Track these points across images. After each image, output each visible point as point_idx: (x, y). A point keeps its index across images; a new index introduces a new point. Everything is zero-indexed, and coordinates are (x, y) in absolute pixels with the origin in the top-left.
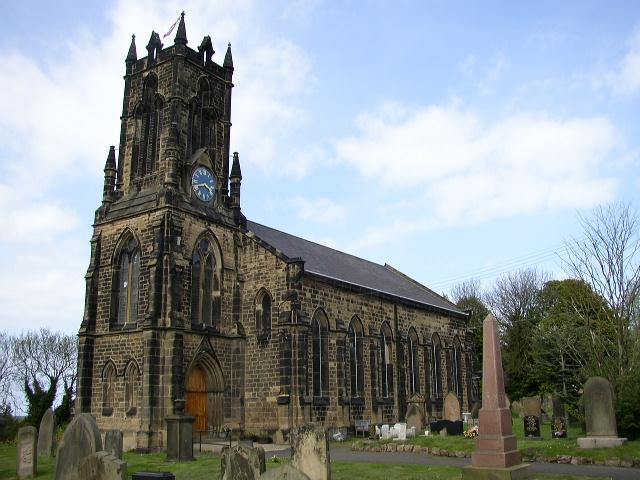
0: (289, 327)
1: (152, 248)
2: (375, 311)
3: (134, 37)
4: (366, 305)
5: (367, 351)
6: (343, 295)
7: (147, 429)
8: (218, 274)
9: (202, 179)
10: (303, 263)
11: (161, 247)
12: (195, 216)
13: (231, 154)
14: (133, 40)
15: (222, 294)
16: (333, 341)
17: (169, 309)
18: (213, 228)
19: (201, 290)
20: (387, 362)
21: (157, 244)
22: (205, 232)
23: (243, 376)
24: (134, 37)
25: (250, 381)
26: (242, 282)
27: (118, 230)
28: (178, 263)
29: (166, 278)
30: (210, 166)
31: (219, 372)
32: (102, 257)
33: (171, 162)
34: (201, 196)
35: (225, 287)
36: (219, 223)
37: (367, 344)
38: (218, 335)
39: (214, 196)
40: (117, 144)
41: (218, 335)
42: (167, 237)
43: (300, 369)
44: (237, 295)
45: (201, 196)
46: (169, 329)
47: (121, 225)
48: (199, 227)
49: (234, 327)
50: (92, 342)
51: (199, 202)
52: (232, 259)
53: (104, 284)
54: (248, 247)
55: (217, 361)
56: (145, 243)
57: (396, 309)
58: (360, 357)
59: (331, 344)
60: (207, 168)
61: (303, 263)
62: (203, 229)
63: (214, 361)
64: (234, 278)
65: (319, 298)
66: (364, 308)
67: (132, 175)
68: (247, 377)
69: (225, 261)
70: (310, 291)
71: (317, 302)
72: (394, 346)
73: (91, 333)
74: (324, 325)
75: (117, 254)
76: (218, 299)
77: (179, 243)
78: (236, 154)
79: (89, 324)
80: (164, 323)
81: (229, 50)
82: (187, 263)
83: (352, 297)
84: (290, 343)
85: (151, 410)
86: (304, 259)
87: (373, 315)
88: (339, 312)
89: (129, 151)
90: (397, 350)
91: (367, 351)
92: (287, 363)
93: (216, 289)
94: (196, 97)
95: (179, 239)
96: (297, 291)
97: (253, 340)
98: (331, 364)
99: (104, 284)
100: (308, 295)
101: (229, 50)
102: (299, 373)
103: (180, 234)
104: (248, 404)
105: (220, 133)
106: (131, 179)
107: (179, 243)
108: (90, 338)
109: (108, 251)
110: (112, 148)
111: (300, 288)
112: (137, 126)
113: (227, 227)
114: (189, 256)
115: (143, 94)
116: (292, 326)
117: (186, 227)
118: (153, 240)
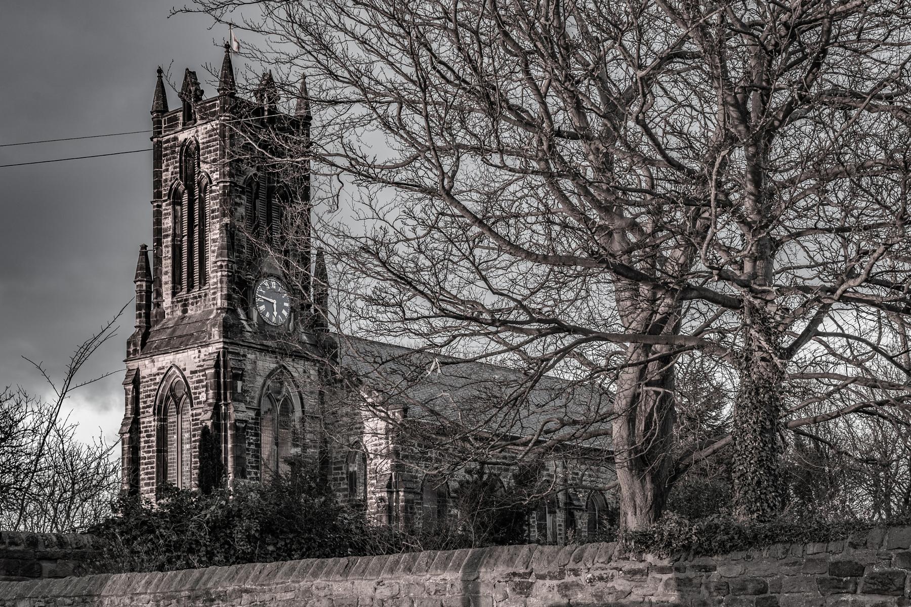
1: (204, 394)
3: (160, 71)
9: (271, 293)
11: (218, 396)
14: (160, 77)
17: (231, 477)
18: (288, 363)
19: (312, 290)
21: (211, 392)
22: (277, 369)
24: (160, 71)
27: (160, 369)
29: (226, 436)
32: (141, 405)
33: (225, 279)
39: (290, 315)
47: (164, 360)
48: (267, 364)
53: (146, 442)
56: (196, 388)
62: (273, 366)
67: (174, 288)
77: (239, 390)
82: (252, 414)
95: (239, 383)
99: (146, 442)
106: (174, 294)
107: (239, 390)
109: (149, 396)
115: (181, 167)
117: (249, 367)
118: (206, 386)
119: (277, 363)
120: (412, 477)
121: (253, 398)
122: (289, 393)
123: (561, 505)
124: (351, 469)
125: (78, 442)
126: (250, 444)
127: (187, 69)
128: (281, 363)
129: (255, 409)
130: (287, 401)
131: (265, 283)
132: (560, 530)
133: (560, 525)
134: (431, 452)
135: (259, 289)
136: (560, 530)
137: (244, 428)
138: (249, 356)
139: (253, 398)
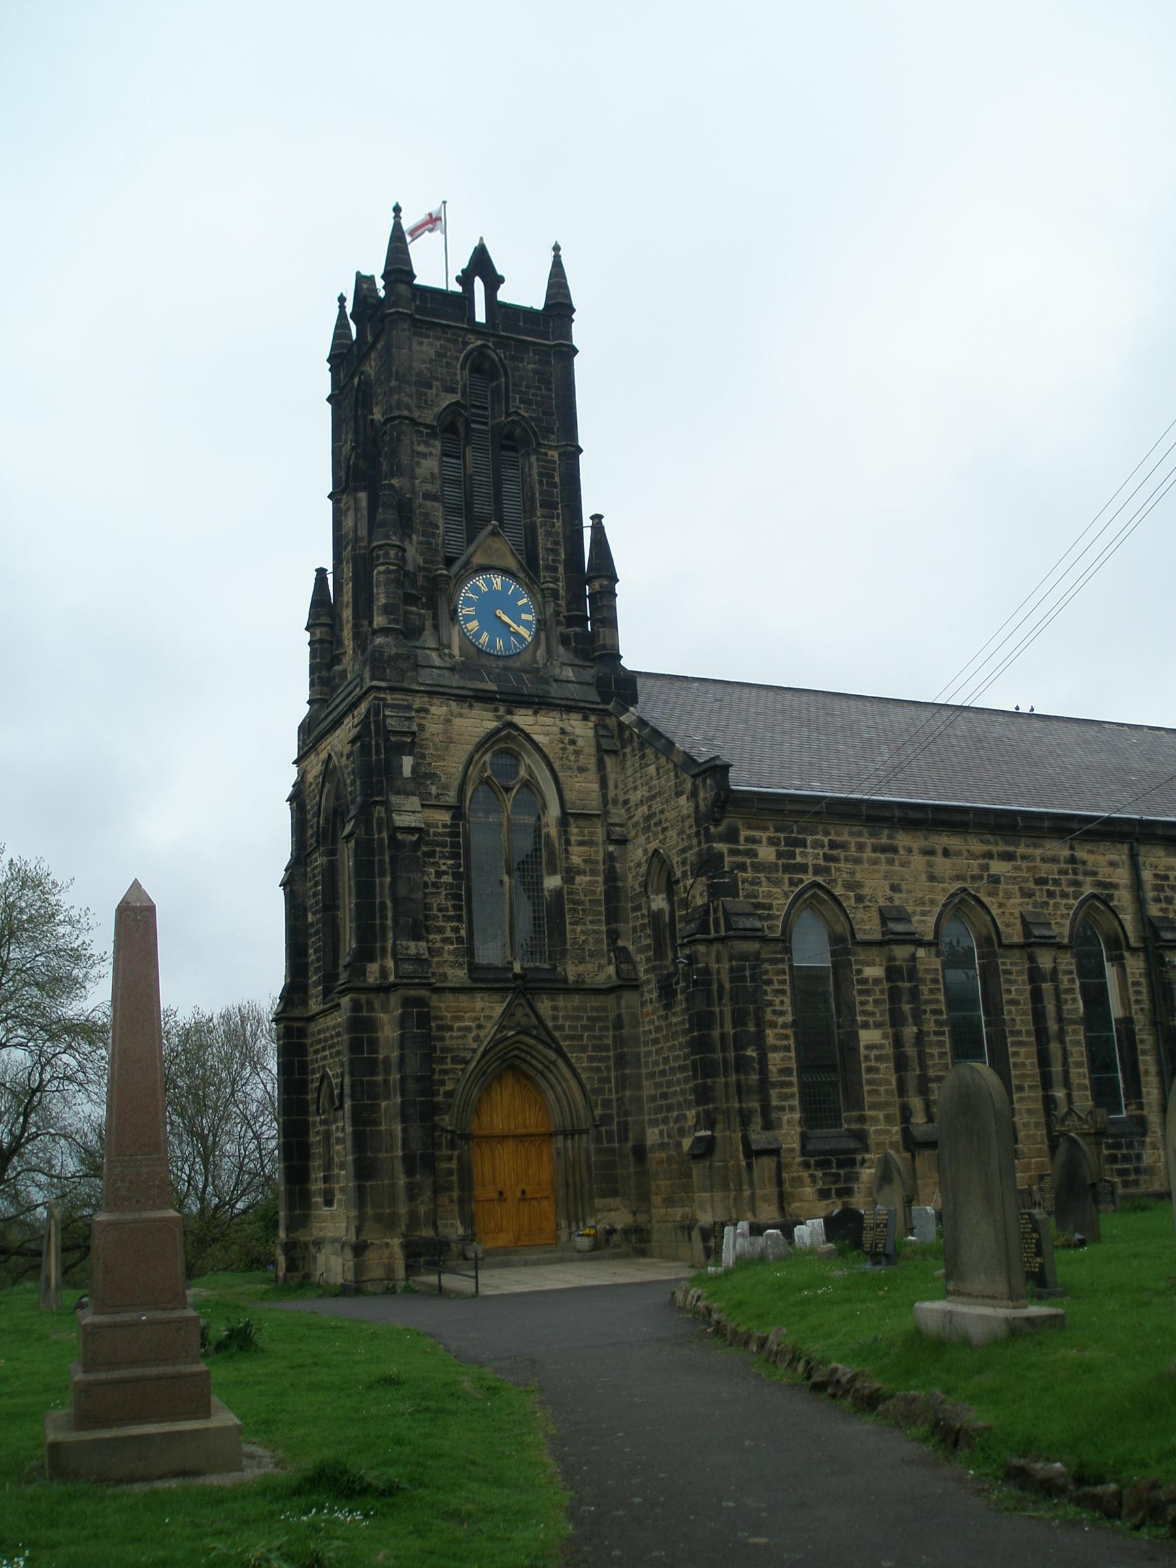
0: (702, 949)
2: (1047, 870)
3: (557, 248)
4: (1008, 857)
5: (1016, 988)
6: (903, 839)
7: (353, 1238)
8: (553, 831)
10: (726, 768)
12: (460, 699)
13: (587, 522)
15: (569, 879)
16: (874, 972)
18: (523, 719)
20: (1116, 1010)
22: (497, 731)
23: (639, 1086)
24: (557, 248)
25: (653, 1098)
26: (622, 842)
28: (401, 820)
30: (512, 564)
31: (574, 1084)
34: (492, 643)
35: (576, 860)
36: (540, 703)
37: (1013, 967)
38: (560, 987)
39: (536, 637)
40: (329, 565)
41: (560, 987)
42: (378, 761)
43: (737, 1057)
44: (611, 877)
45: (492, 643)
46: (394, 986)
49: (610, 963)
50: (302, 1033)
51: (484, 661)
52: (596, 786)
54: (628, 750)
55: (560, 1052)
57: (1133, 857)
58: (994, 1007)
59: (864, 981)
60: (505, 572)
61: (726, 768)
62: (492, 725)
63: (552, 1055)
64: (600, 833)
65: (809, 856)
66: (998, 867)
68: (648, 1089)
69: (568, 795)
70: (772, 842)
71: (803, 868)
72: (1135, 965)
73: (296, 1013)
74: (839, 929)
75: (327, 820)
76: (558, 893)
77: (407, 771)
78: (597, 518)
79: (293, 993)
80: (383, 972)
81: (557, 265)
82: (445, 817)
83: (945, 840)
84: (709, 992)
85: (360, 1190)
86: (726, 759)
87: (1041, 881)
88: (895, 888)
89: (348, 571)
90: (1148, 974)
91: (1016, 988)
92: (701, 1044)
93: (553, 871)
94: (457, 403)
95: (407, 762)
96: (721, 847)
97: (651, 992)
98: (867, 1036)
100: (767, 853)
101: (557, 265)
102: (738, 1072)
103: (410, 749)
104: (655, 1156)
105: (547, 475)
108: (296, 1025)
110: (321, 573)
111: (731, 836)
112: (357, 510)
113: (569, 709)
114: (451, 798)
116: (711, 942)
117: (433, 729)
119: (499, 718)
120: (757, 906)
121: (446, 787)
122: (531, 773)
123: (1133, 942)
124: (654, 906)
125: (231, 1009)
126: (439, 874)
127: (358, 273)
128: (509, 717)
129: (447, 808)
130: (530, 785)
131: (480, 581)
132: (1138, 993)
133: (1135, 984)
134: (803, 854)
135: (466, 592)
136: (1138, 993)
137: (416, 845)
138: (433, 710)
139: (446, 787)
